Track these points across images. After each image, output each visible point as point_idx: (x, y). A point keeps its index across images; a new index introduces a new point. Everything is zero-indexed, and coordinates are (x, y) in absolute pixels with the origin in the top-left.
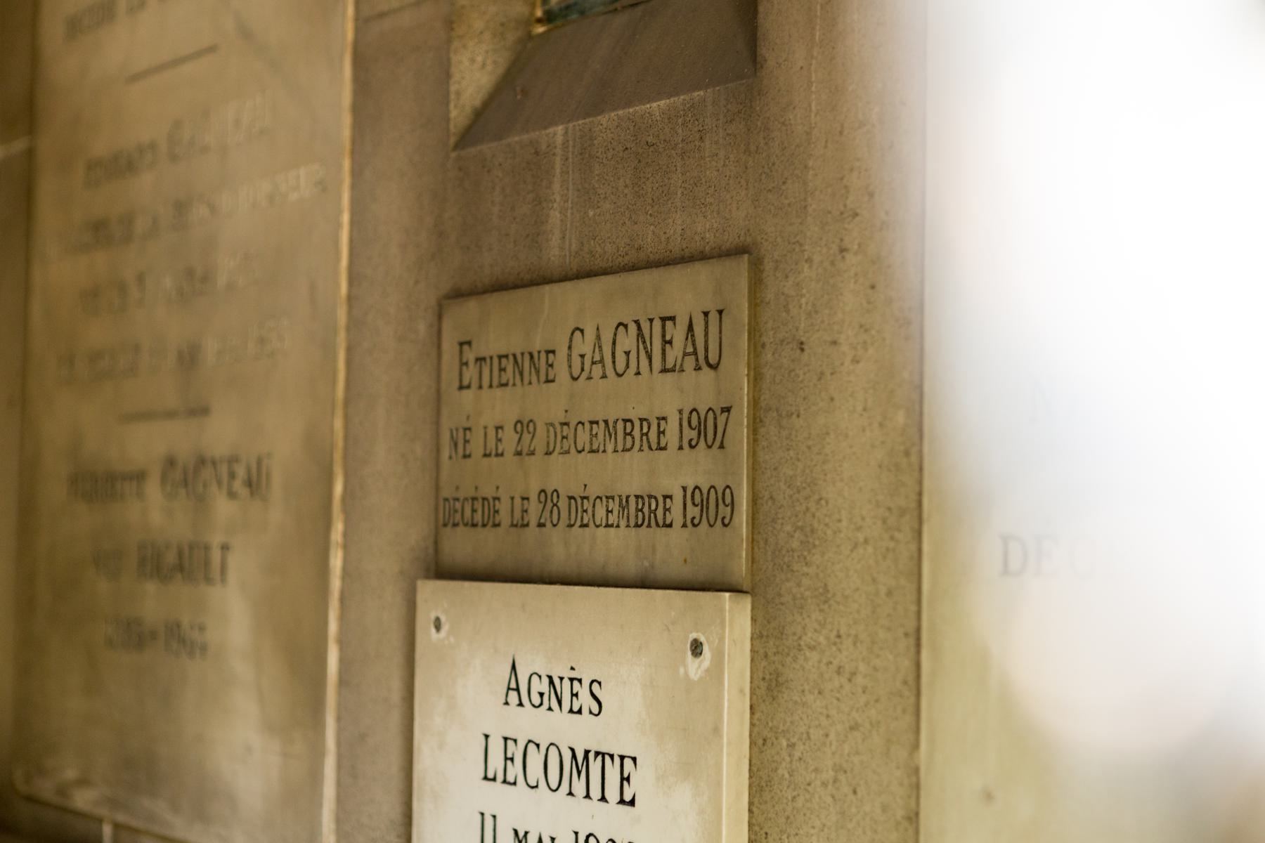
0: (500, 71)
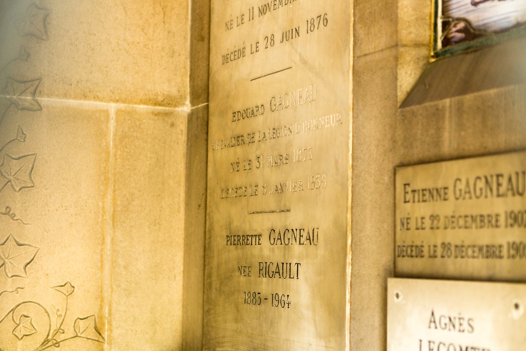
0: (417, 76)
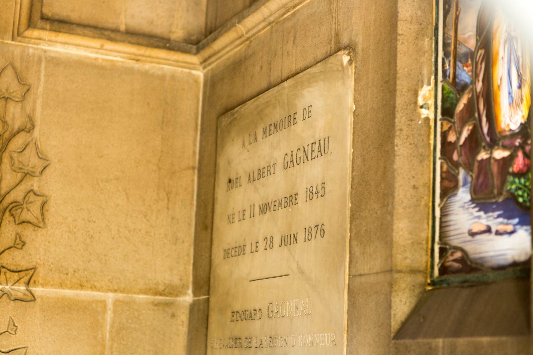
0: (412, 306)
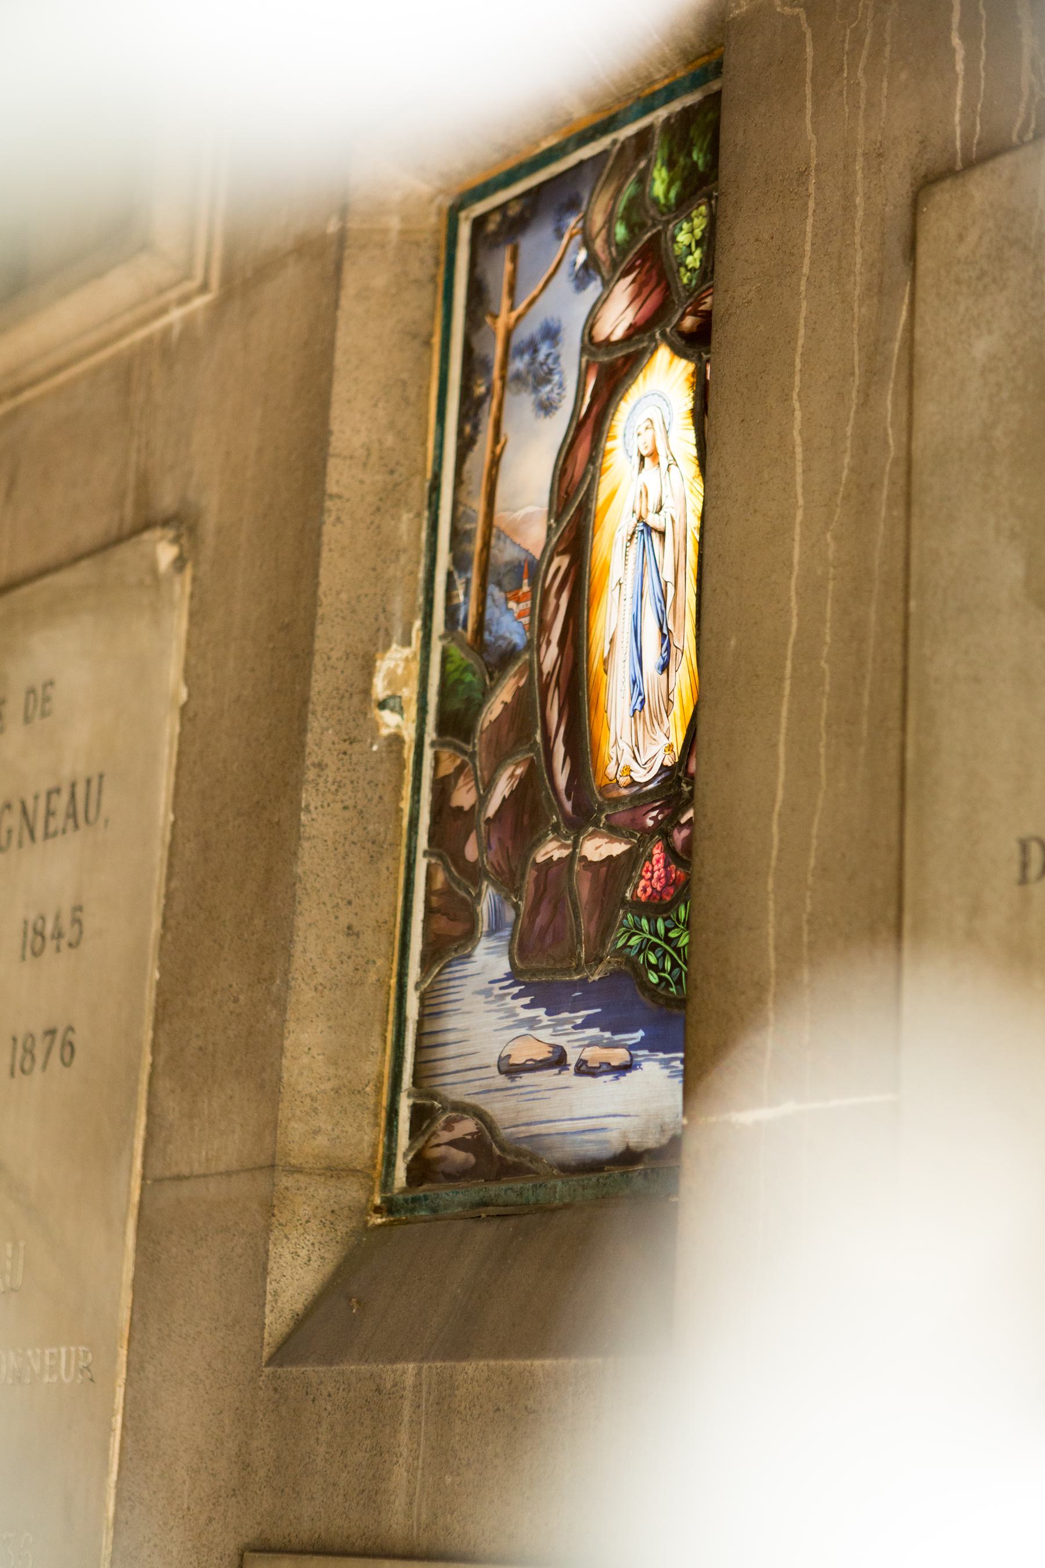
0: (329, 1268)
